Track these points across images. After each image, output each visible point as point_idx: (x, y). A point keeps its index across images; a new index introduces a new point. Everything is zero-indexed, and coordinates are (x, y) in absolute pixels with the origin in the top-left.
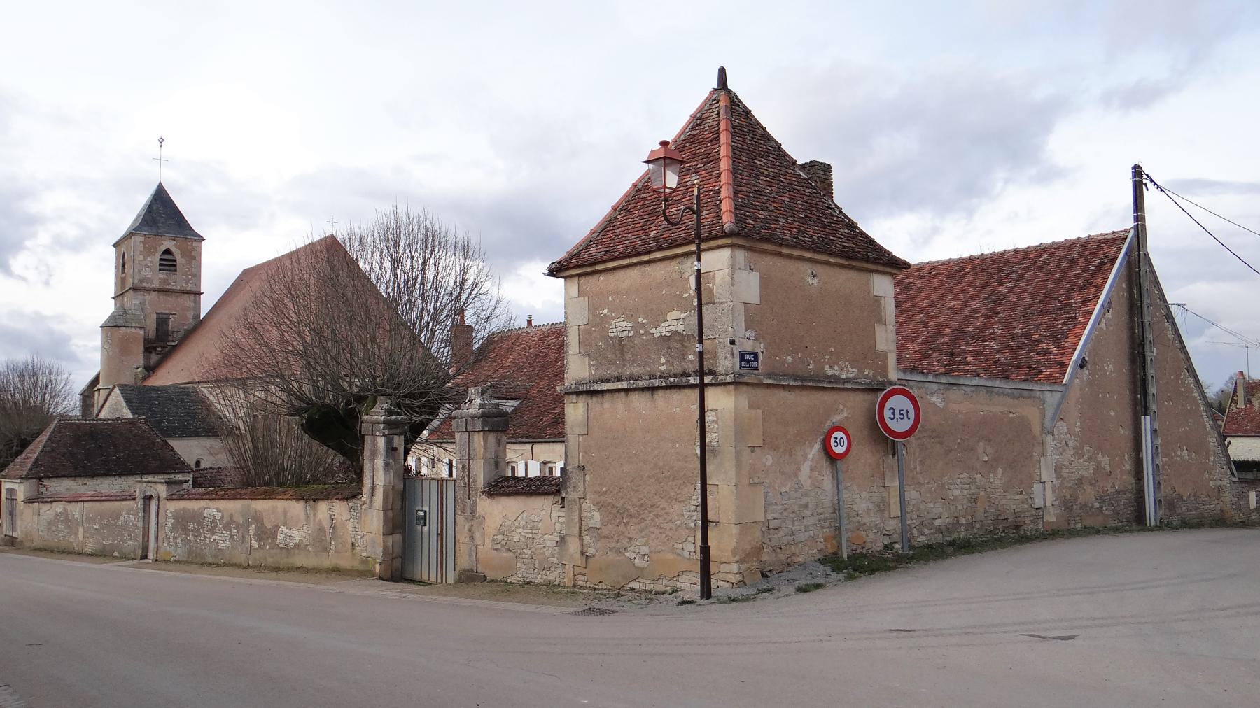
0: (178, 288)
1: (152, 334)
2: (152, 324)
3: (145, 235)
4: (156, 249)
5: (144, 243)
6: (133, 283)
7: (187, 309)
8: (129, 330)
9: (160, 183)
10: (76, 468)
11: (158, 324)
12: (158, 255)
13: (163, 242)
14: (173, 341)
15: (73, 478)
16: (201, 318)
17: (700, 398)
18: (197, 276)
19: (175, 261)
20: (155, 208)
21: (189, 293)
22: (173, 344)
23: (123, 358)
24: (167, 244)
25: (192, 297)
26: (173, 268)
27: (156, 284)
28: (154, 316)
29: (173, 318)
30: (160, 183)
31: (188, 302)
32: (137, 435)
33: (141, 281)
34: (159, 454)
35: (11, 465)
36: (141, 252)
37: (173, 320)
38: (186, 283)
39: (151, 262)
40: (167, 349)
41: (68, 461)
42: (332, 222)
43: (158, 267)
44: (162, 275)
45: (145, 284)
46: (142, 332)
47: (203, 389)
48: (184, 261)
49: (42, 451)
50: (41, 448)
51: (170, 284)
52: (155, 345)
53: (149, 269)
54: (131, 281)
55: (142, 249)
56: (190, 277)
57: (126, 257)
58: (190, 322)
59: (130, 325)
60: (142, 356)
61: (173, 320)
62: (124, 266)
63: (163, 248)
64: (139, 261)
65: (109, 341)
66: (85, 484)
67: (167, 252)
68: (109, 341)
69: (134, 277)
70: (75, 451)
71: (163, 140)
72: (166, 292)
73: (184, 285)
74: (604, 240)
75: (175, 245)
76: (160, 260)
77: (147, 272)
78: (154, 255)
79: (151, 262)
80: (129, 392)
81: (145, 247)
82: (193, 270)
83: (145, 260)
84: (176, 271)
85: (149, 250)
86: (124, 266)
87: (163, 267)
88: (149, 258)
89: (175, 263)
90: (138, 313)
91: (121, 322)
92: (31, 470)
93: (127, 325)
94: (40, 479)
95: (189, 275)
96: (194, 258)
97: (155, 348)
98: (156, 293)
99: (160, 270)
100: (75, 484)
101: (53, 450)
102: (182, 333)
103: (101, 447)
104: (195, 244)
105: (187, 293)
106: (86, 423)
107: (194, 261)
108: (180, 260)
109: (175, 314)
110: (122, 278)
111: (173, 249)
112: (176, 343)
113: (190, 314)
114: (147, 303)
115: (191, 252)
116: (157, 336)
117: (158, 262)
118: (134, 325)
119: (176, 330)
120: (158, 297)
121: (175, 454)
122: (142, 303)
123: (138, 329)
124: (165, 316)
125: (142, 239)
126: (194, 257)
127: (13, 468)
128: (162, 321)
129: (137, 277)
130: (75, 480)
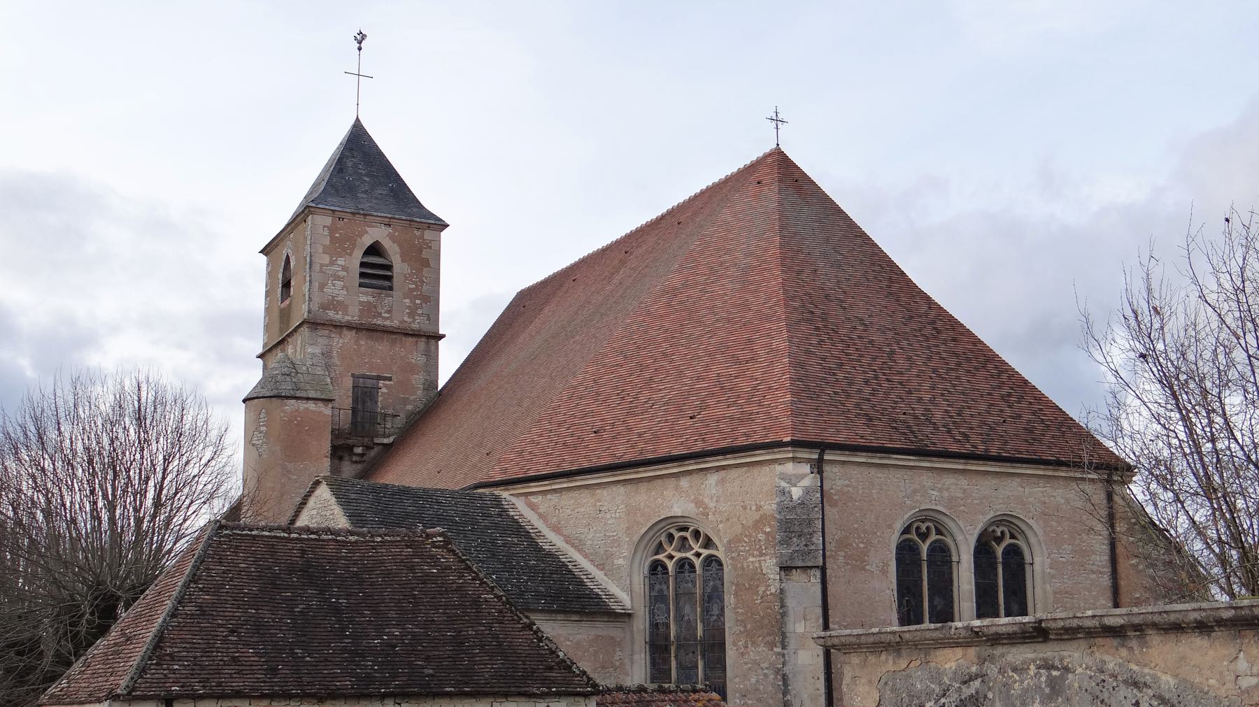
0: (396, 323)
1: (345, 418)
2: (344, 396)
4: (354, 246)
5: (332, 230)
6: (309, 312)
7: (411, 369)
8: (303, 405)
9: (357, 119)
10: (274, 671)
11: (355, 400)
12: (358, 256)
13: (368, 229)
14: (384, 436)
16: (439, 389)
18: (430, 300)
19: (389, 267)
20: (350, 164)
21: (416, 335)
22: (386, 441)
23: (290, 466)
24: (376, 233)
25: (422, 344)
26: (387, 283)
27: (352, 315)
28: (348, 382)
29: (386, 386)
30: (357, 119)
31: (413, 353)
32: (426, 579)
33: (324, 307)
34: (496, 637)
35: (77, 666)
37: (384, 390)
38: (412, 314)
39: (344, 268)
40: (372, 453)
41: (248, 645)
42: (777, 120)
43: (357, 280)
44: (366, 296)
45: (331, 314)
46: (327, 410)
47: (514, 500)
49: (173, 614)
50: (169, 604)
51: (380, 315)
52: (350, 442)
53: (339, 284)
54: (305, 307)
55: (327, 241)
56: (418, 302)
57: (292, 264)
58: (417, 398)
59: (303, 394)
60: (327, 463)
61: (384, 390)
62: (287, 285)
63: (367, 241)
64: (322, 265)
65: (263, 428)
67: (374, 249)
68: (263, 428)
69: (310, 299)
70: (266, 615)
71: (364, 37)
72: (373, 330)
73: (406, 319)
75: (391, 237)
76: (363, 265)
77: (335, 290)
78: (350, 255)
79: (344, 268)
80: (353, 496)
83: (332, 263)
84: (391, 288)
85: (339, 245)
86: (287, 285)
87: (367, 281)
88: (341, 261)
89: (389, 273)
90: (319, 371)
91: (286, 388)
92: (142, 670)
93: (298, 394)
95: (416, 297)
96: (425, 263)
97: (350, 449)
98: (354, 332)
99: (360, 286)
101: (203, 611)
102: (400, 422)
103: (337, 610)
104: (428, 235)
105: (413, 335)
106: (289, 540)
108: (400, 268)
109: (390, 379)
110: (282, 311)
111: (387, 244)
112: (391, 439)
113: (418, 379)
114: (335, 354)
115: (420, 250)
116: (354, 423)
117: (356, 269)
118: (312, 394)
119: (390, 411)
120: (357, 342)
121: (540, 640)
122: (327, 354)
123: (320, 404)
124: (369, 383)
125: (328, 221)
127: (82, 672)
128: (364, 394)
129: (317, 300)
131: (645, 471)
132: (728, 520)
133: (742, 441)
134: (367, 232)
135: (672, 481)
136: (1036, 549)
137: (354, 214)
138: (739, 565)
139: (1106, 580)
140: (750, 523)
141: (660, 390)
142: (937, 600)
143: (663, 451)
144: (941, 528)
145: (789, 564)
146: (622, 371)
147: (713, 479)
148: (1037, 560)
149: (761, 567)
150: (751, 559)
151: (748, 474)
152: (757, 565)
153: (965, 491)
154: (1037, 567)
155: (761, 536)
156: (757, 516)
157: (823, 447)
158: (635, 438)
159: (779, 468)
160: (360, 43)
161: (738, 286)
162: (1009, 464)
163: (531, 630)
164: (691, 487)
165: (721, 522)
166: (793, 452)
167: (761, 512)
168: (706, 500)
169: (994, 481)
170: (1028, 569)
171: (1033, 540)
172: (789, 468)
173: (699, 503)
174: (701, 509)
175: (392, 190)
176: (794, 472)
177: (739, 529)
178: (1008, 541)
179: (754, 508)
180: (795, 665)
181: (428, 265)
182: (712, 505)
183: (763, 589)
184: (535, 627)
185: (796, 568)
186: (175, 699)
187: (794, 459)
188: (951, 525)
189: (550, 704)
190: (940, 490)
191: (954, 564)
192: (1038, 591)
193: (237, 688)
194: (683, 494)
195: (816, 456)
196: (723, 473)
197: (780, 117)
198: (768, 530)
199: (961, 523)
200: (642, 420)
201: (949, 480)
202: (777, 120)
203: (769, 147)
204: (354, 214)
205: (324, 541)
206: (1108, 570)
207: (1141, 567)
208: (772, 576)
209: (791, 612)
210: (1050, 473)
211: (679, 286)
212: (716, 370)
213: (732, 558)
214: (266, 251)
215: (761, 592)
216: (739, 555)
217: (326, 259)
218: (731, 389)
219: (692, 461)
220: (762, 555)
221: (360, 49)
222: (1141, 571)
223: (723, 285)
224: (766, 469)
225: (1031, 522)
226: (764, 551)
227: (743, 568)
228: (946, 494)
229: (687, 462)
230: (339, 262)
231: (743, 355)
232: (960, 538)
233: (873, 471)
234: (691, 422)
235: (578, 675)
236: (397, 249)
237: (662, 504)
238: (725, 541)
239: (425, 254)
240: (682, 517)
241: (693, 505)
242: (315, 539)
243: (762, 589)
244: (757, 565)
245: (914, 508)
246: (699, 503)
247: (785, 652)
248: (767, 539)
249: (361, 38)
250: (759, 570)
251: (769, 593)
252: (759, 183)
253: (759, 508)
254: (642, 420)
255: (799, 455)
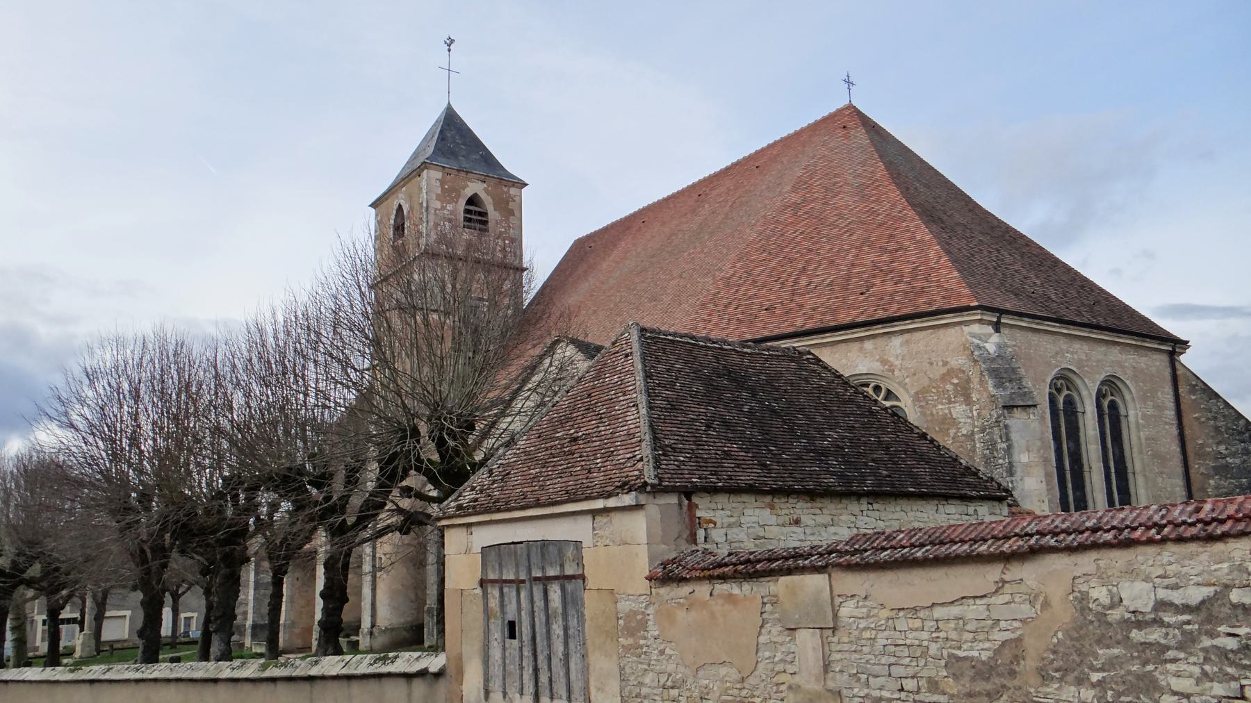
3: (444, 167)
4: (458, 196)
5: (442, 182)
13: (469, 183)
15: (768, 499)
17: (1106, 484)
19: (484, 214)
24: (474, 187)
36: (438, 196)
44: (466, 235)
48: (497, 214)
56: (507, 242)
63: (469, 192)
66: (797, 522)
67: (473, 200)
71: (452, 41)
74: (575, 415)
75: (486, 190)
78: (456, 202)
81: (443, 188)
82: (511, 231)
83: (443, 208)
85: (448, 194)
88: (450, 207)
94: (688, 493)
96: (512, 213)
100: (773, 520)
104: (513, 191)
107: (511, 217)
108: (493, 215)
111: (483, 195)
117: (461, 216)
125: (439, 175)
126: (511, 211)
130: (772, 507)
131: (831, 336)
132: (914, 374)
133: (925, 308)
134: (468, 186)
135: (856, 345)
136: (1130, 405)
137: (457, 170)
138: (928, 412)
139: (1175, 431)
140: (938, 377)
141: (818, 275)
142: (1071, 444)
143: (844, 319)
144: (1070, 385)
145: (1011, 403)
146: (773, 264)
147: (897, 341)
148: (1131, 413)
149: (950, 413)
150: (940, 407)
151: (933, 335)
152: (947, 411)
153: (1087, 354)
154: (1132, 419)
155: (949, 387)
156: (944, 370)
157: (1001, 312)
158: (810, 312)
159: (966, 329)
160: (449, 45)
161: (857, 199)
162: (1115, 334)
163: (926, 439)
164: (876, 348)
165: (907, 377)
166: (982, 314)
167: (948, 367)
168: (891, 359)
169: (1103, 349)
170: (1123, 420)
171: (1128, 397)
172: (976, 328)
173: (884, 362)
174: (886, 367)
175: (482, 155)
176: (980, 332)
177: (926, 382)
178: (1110, 398)
179: (940, 363)
180: (1023, 490)
181: (513, 214)
182: (897, 363)
183: (954, 431)
184: (929, 437)
185: (1017, 407)
186: (693, 492)
187: (980, 321)
188: (1078, 382)
189: (977, 508)
190: (1072, 353)
191: (1080, 415)
192: (1134, 437)
193: (751, 482)
194: (867, 355)
195: (995, 320)
196: (907, 336)
197: (851, 81)
198: (956, 381)
199: (1086, 380)
200: (811, 298)
201: (1077, 345)
202: (849, 82)
203: (841, 103)
204: (457, 170)
205: (726, 350)
206: (1175, 422)
207: (1203, 419)
208: (963, 420)
209: (1015, 444)
210: (1139, 343)
211: (799, 201)
212: (867, 259)
213: (921, 407)
214: (374, 205)
215: (952, 435)
216: (927, 403)
217: (438, 205)
218: (891, 272)
219: (880, 326)
220: (950, 402)
221: (449, 50)
222: (1203, 422)
223: (842, 199)
224: (952, 331)
225: (1128, 382)
226: (953, 400)
227: (932, 414)
228: (1076, 357)
229: (874, 327)
230: (448, 208)
231: (891, 246)
232: (1084, 393)
233: (1030, 335)
234: (861, 298)
235: (987, 481)
236: (491, 201)
237: (847, 364)
238: (913, 392)
239: (511, 205)
240: (866, 374)
241: (878, 364)
242: (719, 348)
243: (952, 432)
244: (947, 411)
245: (1057, 366)
246: (884, 362)
247: (1013, 479)
248: (955, 390)
249: (450, 44)
250: (949, 416)
251: (960, 434)
252: (844, 127)
253: (945, 364)
254: (811, 298)
255: (985, 318)
